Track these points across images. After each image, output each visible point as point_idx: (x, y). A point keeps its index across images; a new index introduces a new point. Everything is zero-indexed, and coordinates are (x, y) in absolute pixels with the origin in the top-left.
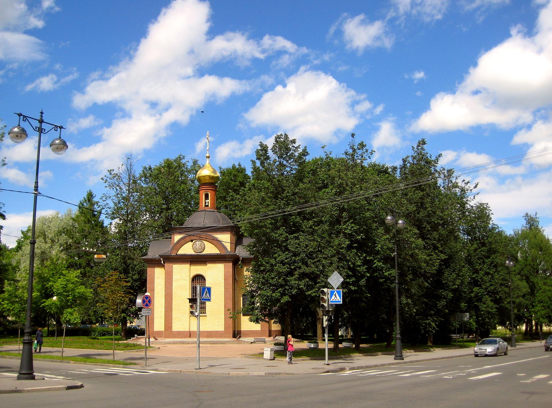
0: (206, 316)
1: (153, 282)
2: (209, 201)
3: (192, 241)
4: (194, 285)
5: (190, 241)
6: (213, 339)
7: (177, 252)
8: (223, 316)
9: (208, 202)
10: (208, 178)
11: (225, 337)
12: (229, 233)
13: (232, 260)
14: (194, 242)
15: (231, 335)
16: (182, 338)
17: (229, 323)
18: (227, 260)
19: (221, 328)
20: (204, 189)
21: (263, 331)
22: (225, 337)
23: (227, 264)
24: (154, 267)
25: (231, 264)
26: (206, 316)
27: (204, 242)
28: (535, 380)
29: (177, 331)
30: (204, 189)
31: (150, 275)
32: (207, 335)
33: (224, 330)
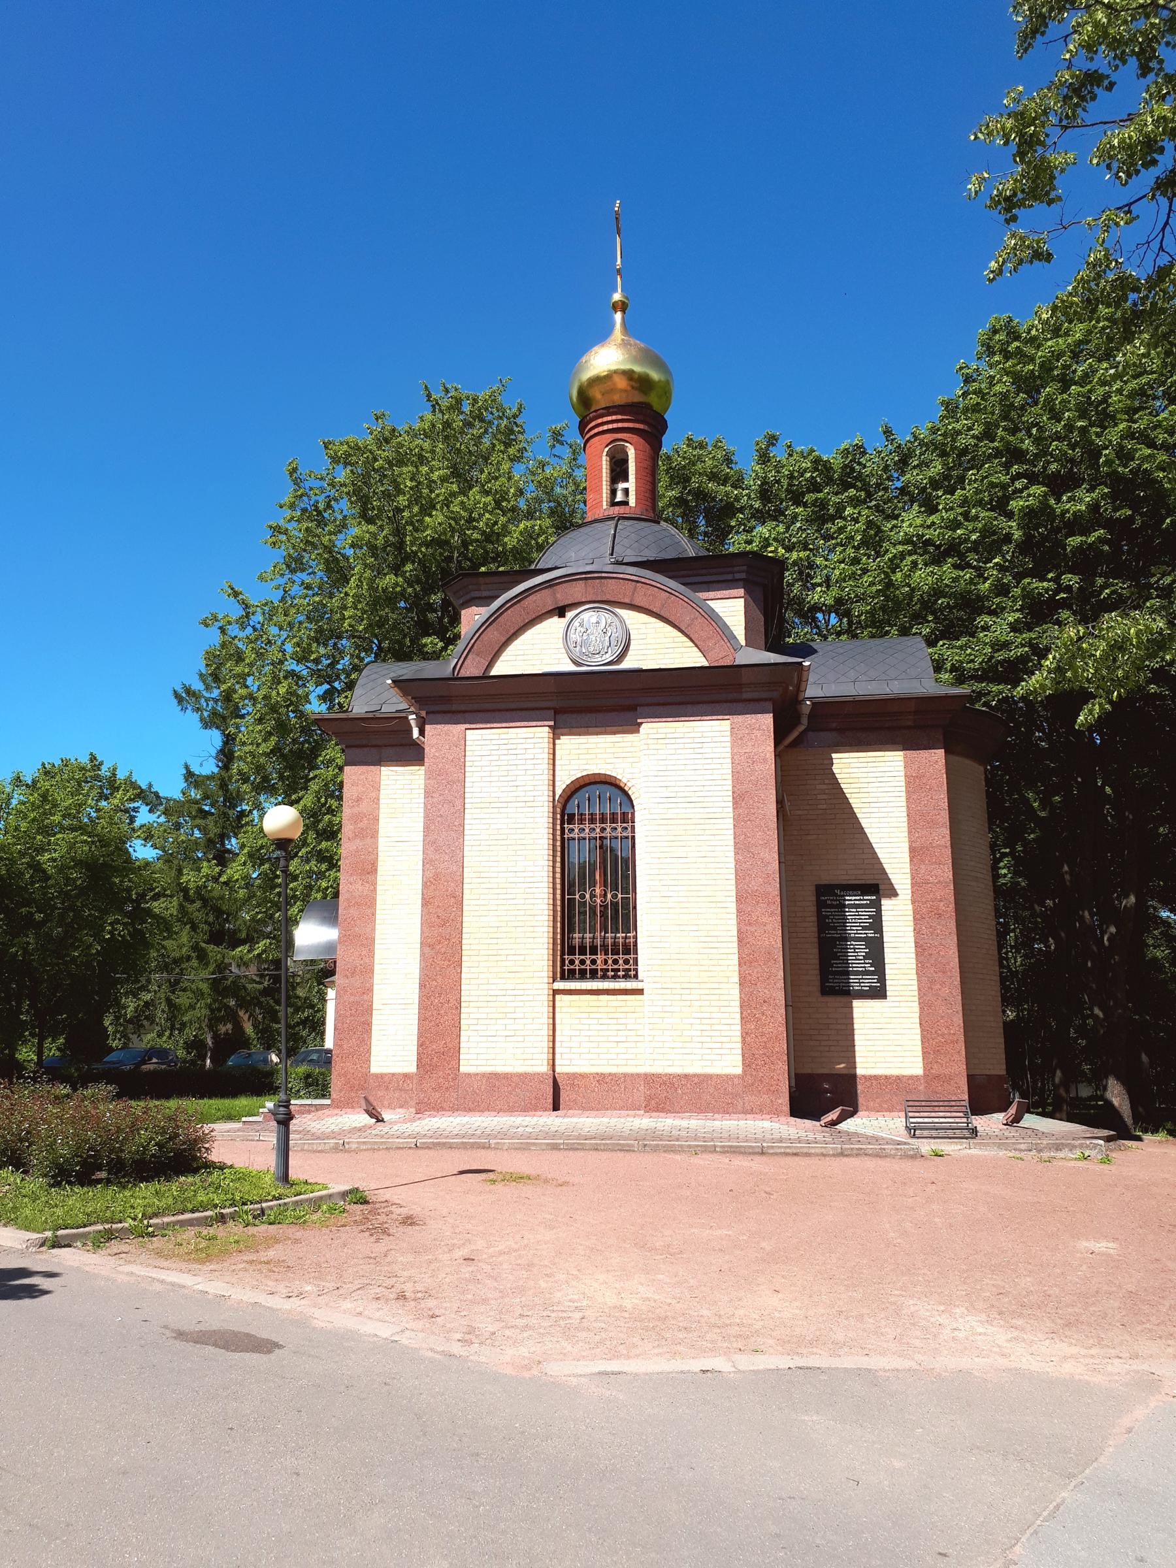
0: (640, 992)
1: (371, 832)
2: (631, 484)
3: (561, 612)
4: (572, 962)
5: (549, 614)
6: (685, 1123)
7: (491, 665)
8: (735, 992)
9: (626, 491)
10: (621, 383)
11: (752, 1112)
12: (741, 592)
13: (775, 695)
14: (570, 615)
15: (784, 1101)
16: (511, 1109)
17: (766, 1030)
18: (745, 696)
19: (730, 1063)
20: (605, 427)
21: (938, 1077)
22: (748, 1112)
23: (750, 719)
24: (379, 762)
25: (766, 721)
26: (640, 992)
27: (624, 613)
28: (126, 1279)
29: (483, 1075)
30: (605, 427)
31: (359, 800)
32: (649, 1099)
33: (738, 1070)
